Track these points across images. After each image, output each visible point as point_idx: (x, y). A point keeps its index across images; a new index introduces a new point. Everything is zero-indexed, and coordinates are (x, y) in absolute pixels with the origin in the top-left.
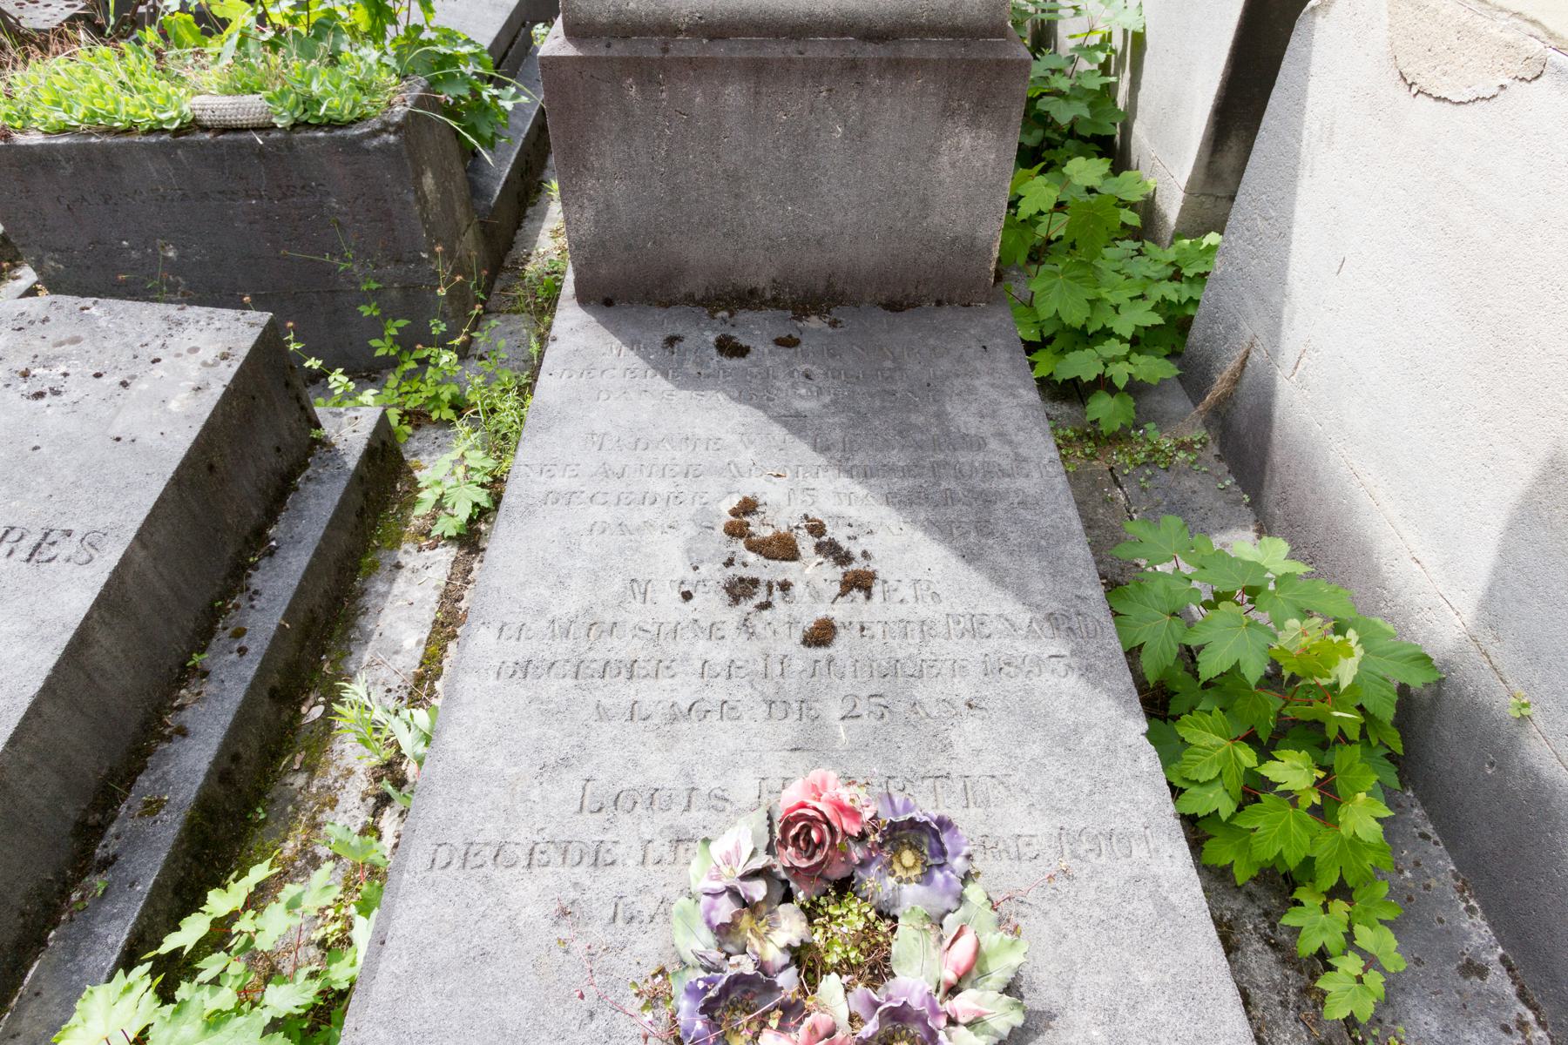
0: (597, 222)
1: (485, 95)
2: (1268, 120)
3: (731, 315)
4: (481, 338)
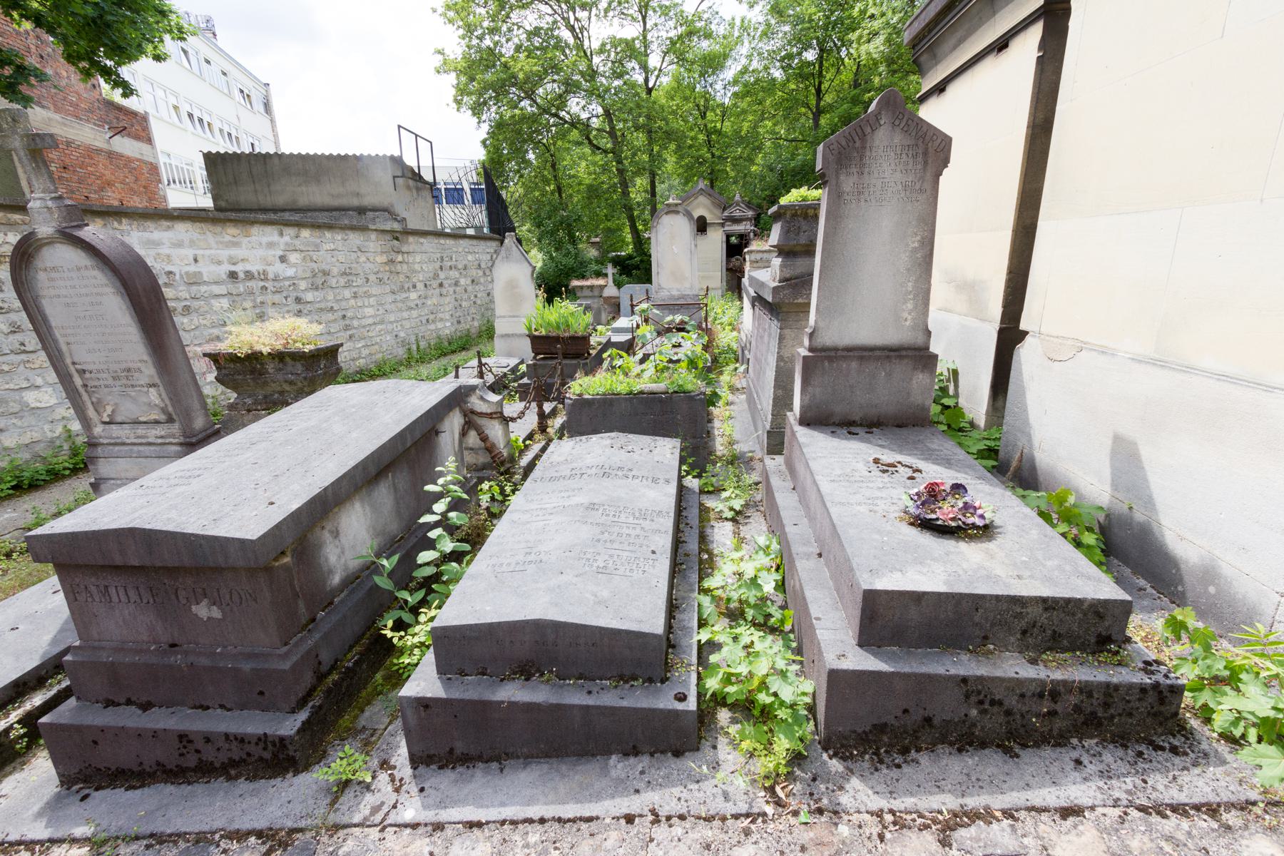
2: (1011, 380)
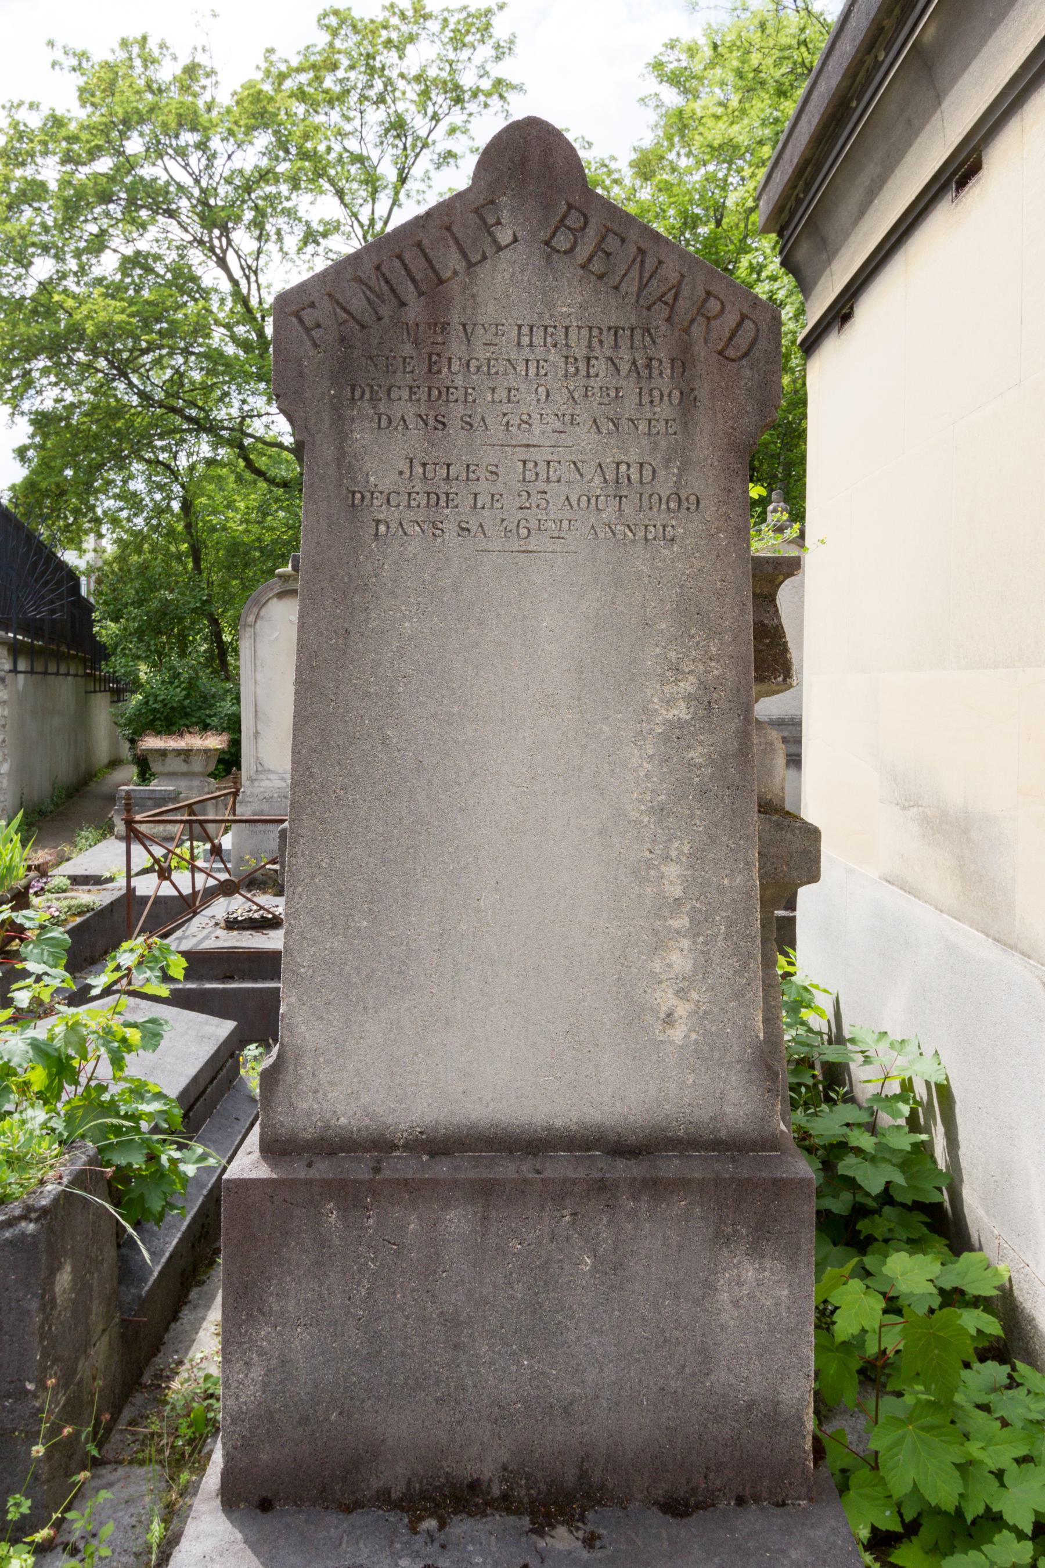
0: (265, 1384)
1: (164, 1159)
3: (442, 1526)
4: (78, 1521)
